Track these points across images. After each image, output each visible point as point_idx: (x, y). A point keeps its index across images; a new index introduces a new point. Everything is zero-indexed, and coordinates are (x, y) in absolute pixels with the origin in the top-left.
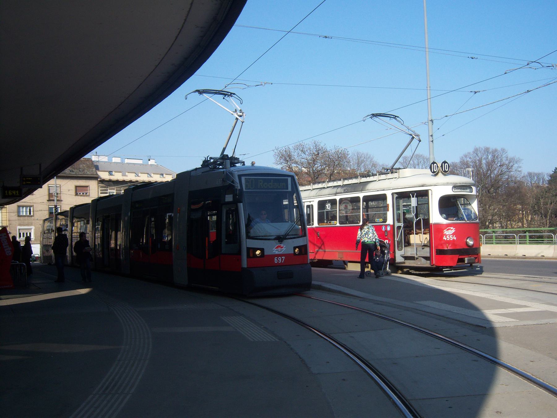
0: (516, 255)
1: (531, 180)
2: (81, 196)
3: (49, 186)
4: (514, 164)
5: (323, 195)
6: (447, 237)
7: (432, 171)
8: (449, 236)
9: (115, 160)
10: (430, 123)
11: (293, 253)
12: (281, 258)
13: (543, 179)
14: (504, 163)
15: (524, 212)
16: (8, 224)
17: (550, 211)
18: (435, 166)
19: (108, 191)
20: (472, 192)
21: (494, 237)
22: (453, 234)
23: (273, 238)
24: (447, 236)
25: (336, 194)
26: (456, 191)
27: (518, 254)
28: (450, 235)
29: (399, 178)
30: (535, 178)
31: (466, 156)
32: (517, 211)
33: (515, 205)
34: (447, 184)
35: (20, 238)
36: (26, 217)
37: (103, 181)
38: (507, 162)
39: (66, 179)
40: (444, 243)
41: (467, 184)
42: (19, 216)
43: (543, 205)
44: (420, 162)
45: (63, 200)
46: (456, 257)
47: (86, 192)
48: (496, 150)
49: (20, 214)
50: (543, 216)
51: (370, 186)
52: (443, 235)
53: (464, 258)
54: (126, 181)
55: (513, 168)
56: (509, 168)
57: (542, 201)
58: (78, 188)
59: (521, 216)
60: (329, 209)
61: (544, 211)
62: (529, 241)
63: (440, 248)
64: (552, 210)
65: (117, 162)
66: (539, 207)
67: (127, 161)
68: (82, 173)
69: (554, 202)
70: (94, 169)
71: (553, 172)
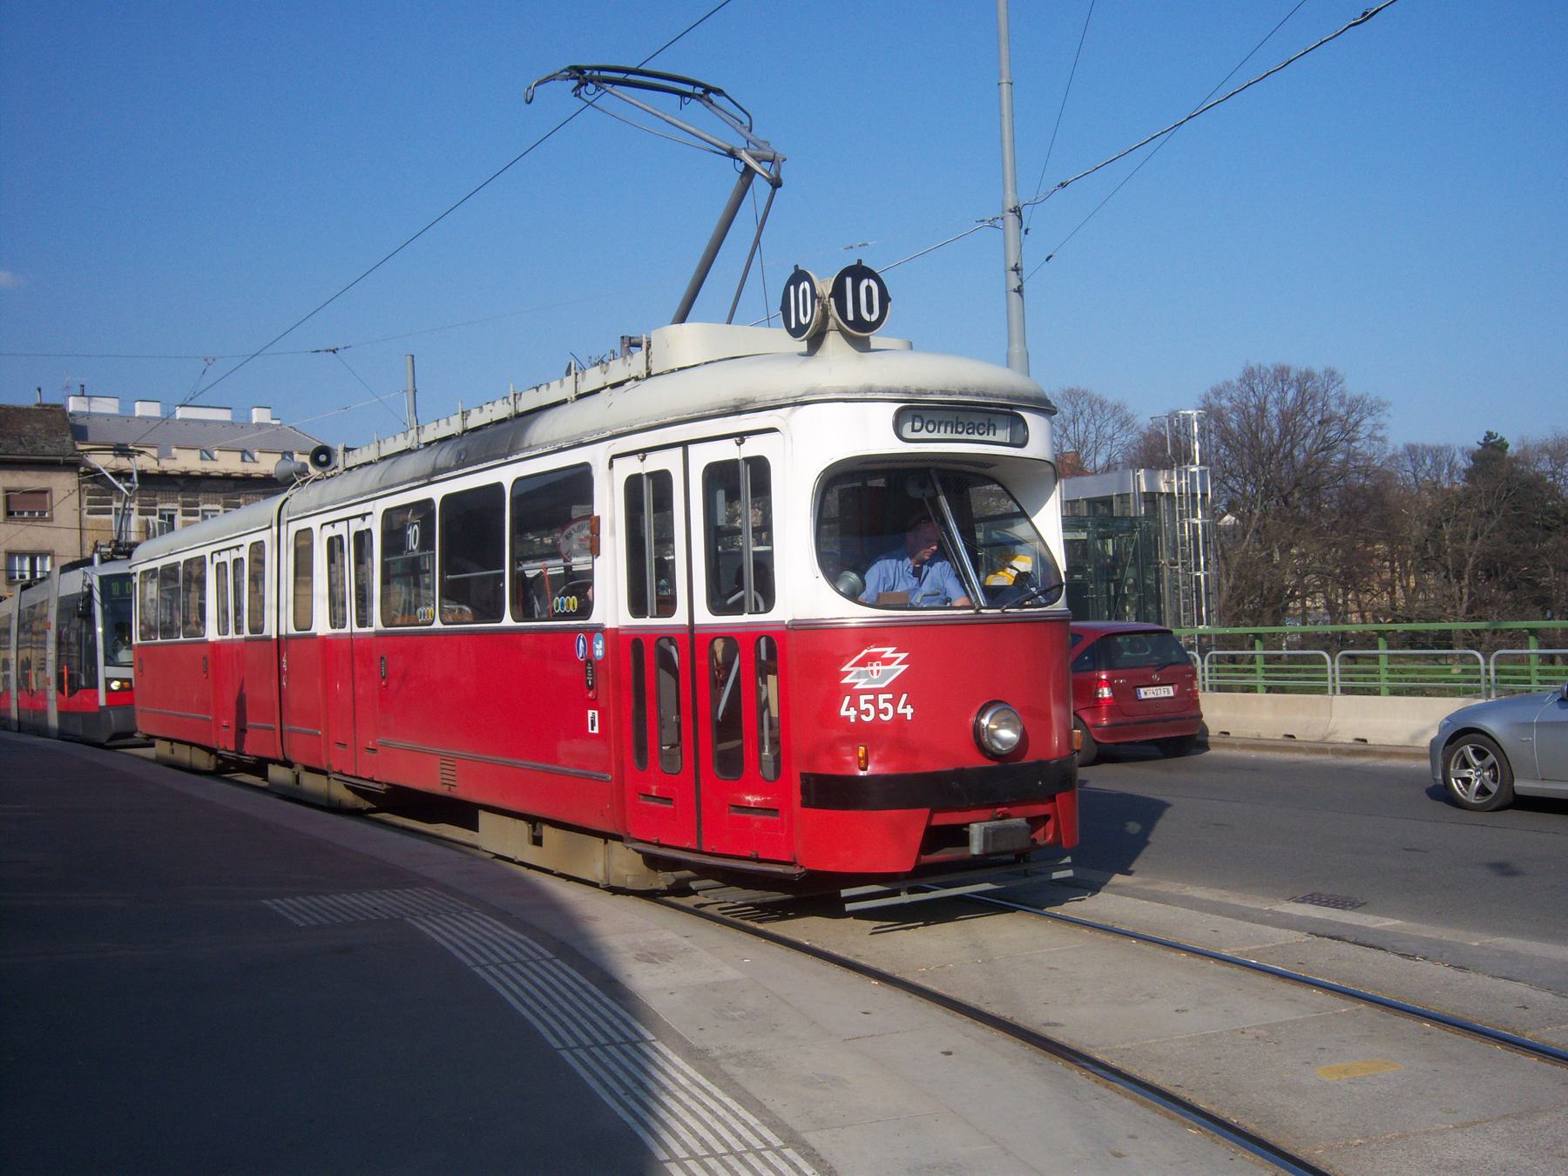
0: (1330, 739)
1: (1415, 468)
2: (25, 520)
4: (1361, 419)
5: (397, 485)
6: (863, 707)
8: (871, 697)
9: (141, 409)
10: (1011, 219)
13: (1450, 464)
14: (1333, 415)
15: (1396, 564)
17: (1471, 559)
18: (804, 291)
19: (111, 504)
20: (1022, 445)
21: (1259, 659)
22: (896, 688)
24: (863, 698)
25: (429, 479)
26: (924, 434)
27: (1336, 732)
28: (876, 692)
29: (649, 375)
30: (1428, 462)
31: (1218, 393)
32: (1375, 560)
33: (1368, 542)
34: (865, 396)
38: (1342, 411)
40: (843, 740)
41: (991, 396)
43: (1452, 541)
44: (1081, 413)
46: (916, 822)
48: (1309, 376)
50: (1451, 576)
51: (544, 430)
52: (838, 692)
53: (967, 825)
54: (169, 473)
55: (1361, 429)
56: (1349, 432)
57: (1447, 529)
59: (1387, 576)
60: (414, 547)
61: (1452, 561)
62: (1391, 671)
63: (826, 767)
64: (1478, 558)
66: (1439, 549)
67: (180, 413)
69: (1482, 534)
70: (69, 438)
71: (1481, 444)
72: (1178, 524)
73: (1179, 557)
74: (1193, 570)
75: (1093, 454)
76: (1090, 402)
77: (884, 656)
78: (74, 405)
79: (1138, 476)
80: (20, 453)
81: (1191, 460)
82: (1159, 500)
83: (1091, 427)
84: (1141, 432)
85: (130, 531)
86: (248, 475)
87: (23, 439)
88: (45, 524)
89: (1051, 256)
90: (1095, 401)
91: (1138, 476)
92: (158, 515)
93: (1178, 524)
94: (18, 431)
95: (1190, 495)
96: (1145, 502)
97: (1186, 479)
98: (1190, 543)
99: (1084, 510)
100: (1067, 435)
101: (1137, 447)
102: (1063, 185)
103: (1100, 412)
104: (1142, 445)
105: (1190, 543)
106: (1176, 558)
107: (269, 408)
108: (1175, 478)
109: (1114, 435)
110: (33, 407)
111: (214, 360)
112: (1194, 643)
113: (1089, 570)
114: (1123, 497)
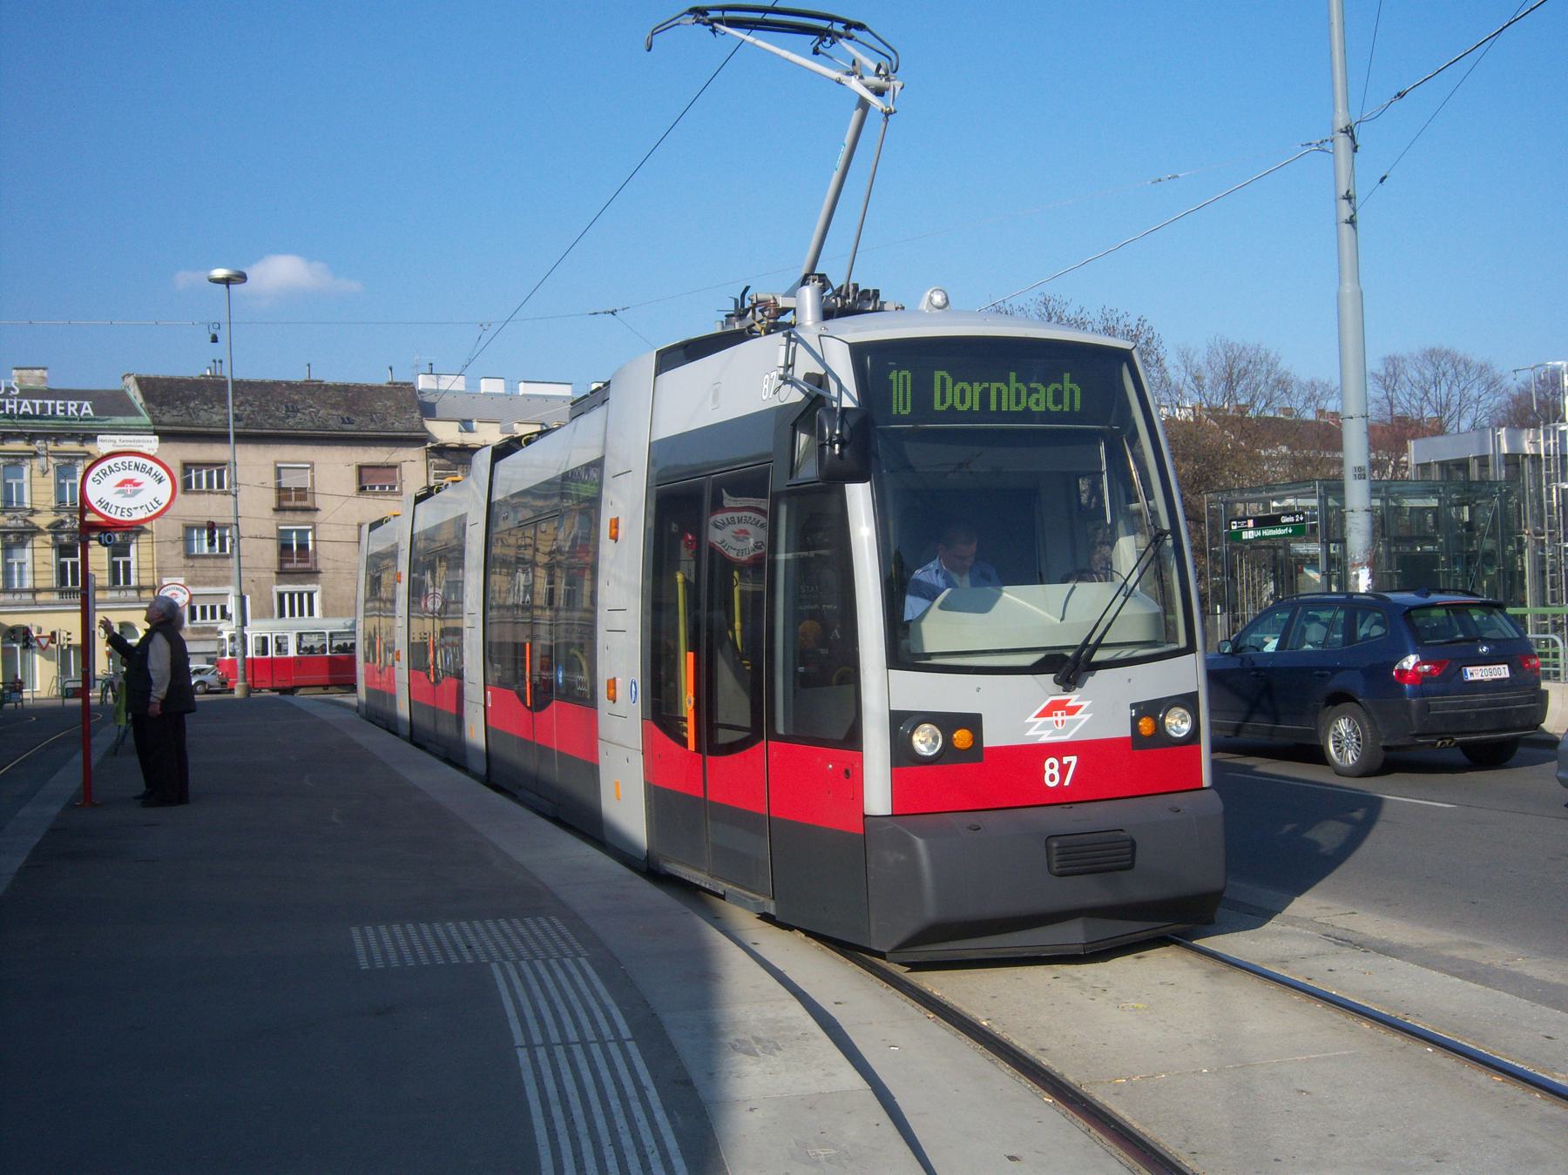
2: (376, 494)
3: (278, 465)
9: (487, 386)
10: (1343, 142)
11: (1128, 734)
12: (1060, 761)
16: (156, 579)
23: (1028, 660)
35: (194, 622)
36: (212, 560)
37: (441, 450)
39: (328, 445)
42: (189, 555)
44: (1444, 375)
45: (320, 508)
47: (391, 483)
49: (194, 551)
58: (365, 472)
65: (491, 394)
67: (523, 389)
68: (378, 427)
70: (417, 415)
72: (1544, 489)
73: (1546, 525)
74: (1562, 540)
75: (1457, 418)
76: (1454, 362)
77: (1068, 705)
78: (423, 383)
79: (1499, 436)
80: (372, 429)
81: (1560, 418)
82: (1523, 463)
83: (1455, 389)
84: (1510, 395)
86: (463, 445)
87: (374, 416)
88: (395, 498)
89: (1385, 178)
90: (1459, 361)
91: (1499, 436)
93: (1544, 489)
94: (369, 408)
95: (1559, 457)
96: (1506, 465)
97: (1555, 438)
98: (1558, 511)
99: (1436, 475)
100: (1428, 399)
101: (1506, 409)
102: (1400, 95)
103: (1464, 373)
104: (1510, 408)
105: (1558, 511)
106: (1542, 527)
107: (570, 384)
108: (1542, 438)
109: (1480, 397)
110: (385, 385)
111: (490, 325)
112: (1562, 623)
113: (1441, 540)
114: (1483, 461)
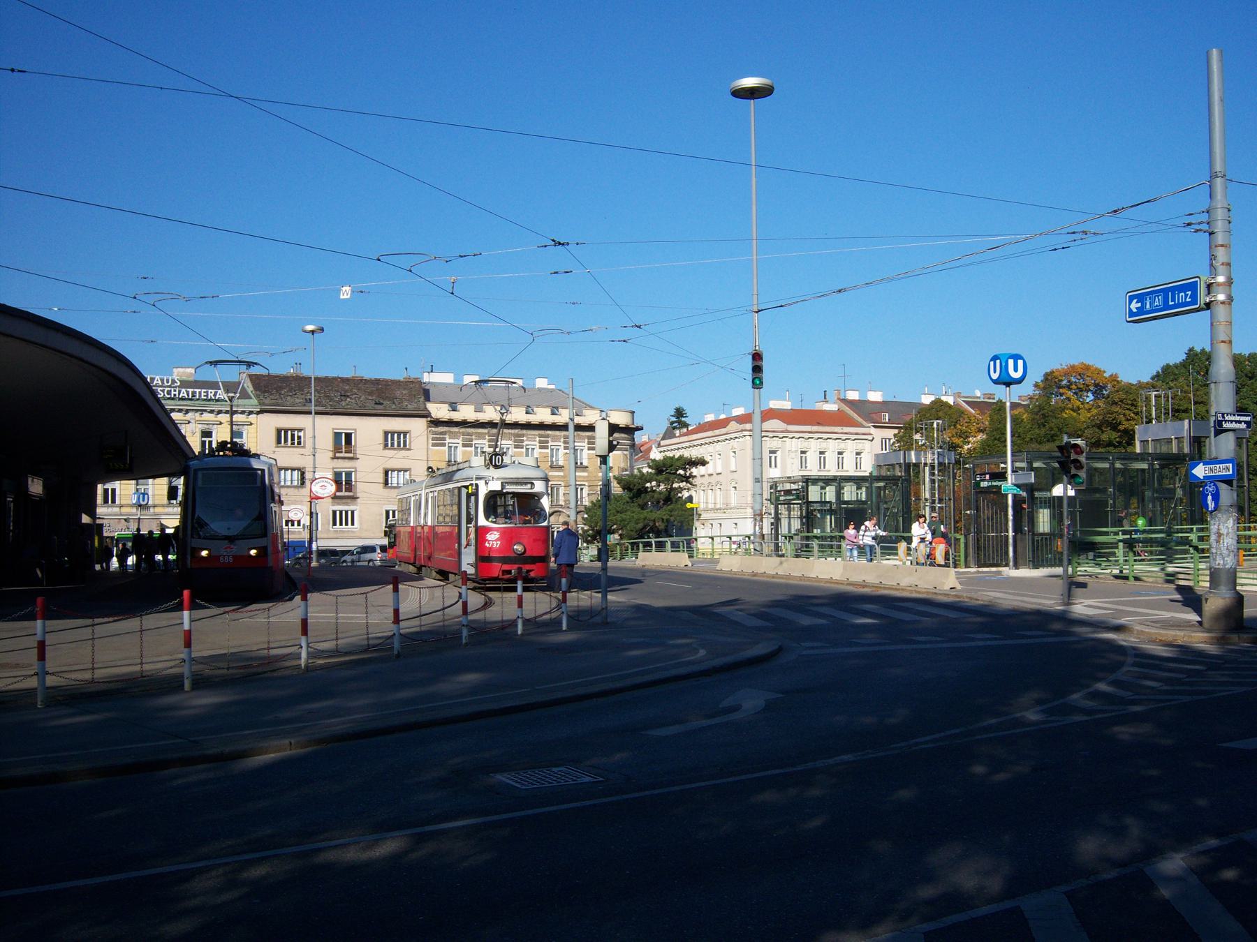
7: (494, 464)
37: (437, 423)
51: (458, 476)
70: (422, 399)
78: (426, 378)
85: (368, 645)
92: (473, 447)
